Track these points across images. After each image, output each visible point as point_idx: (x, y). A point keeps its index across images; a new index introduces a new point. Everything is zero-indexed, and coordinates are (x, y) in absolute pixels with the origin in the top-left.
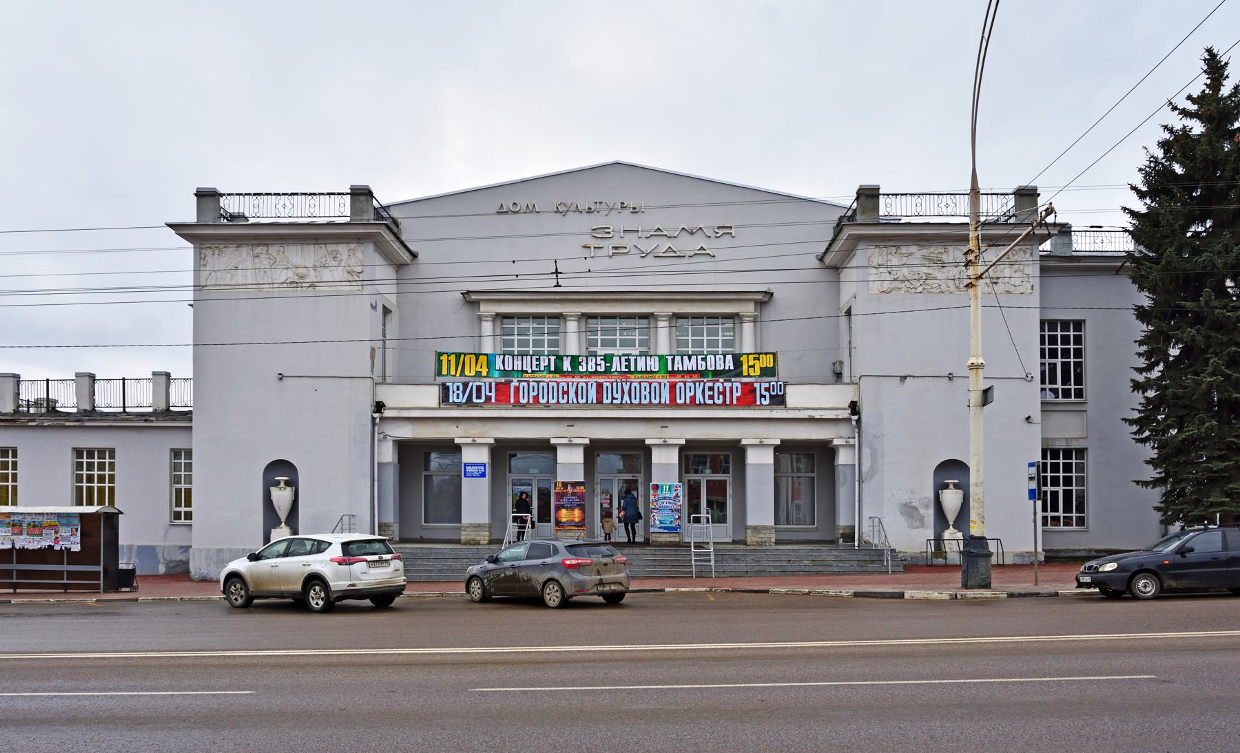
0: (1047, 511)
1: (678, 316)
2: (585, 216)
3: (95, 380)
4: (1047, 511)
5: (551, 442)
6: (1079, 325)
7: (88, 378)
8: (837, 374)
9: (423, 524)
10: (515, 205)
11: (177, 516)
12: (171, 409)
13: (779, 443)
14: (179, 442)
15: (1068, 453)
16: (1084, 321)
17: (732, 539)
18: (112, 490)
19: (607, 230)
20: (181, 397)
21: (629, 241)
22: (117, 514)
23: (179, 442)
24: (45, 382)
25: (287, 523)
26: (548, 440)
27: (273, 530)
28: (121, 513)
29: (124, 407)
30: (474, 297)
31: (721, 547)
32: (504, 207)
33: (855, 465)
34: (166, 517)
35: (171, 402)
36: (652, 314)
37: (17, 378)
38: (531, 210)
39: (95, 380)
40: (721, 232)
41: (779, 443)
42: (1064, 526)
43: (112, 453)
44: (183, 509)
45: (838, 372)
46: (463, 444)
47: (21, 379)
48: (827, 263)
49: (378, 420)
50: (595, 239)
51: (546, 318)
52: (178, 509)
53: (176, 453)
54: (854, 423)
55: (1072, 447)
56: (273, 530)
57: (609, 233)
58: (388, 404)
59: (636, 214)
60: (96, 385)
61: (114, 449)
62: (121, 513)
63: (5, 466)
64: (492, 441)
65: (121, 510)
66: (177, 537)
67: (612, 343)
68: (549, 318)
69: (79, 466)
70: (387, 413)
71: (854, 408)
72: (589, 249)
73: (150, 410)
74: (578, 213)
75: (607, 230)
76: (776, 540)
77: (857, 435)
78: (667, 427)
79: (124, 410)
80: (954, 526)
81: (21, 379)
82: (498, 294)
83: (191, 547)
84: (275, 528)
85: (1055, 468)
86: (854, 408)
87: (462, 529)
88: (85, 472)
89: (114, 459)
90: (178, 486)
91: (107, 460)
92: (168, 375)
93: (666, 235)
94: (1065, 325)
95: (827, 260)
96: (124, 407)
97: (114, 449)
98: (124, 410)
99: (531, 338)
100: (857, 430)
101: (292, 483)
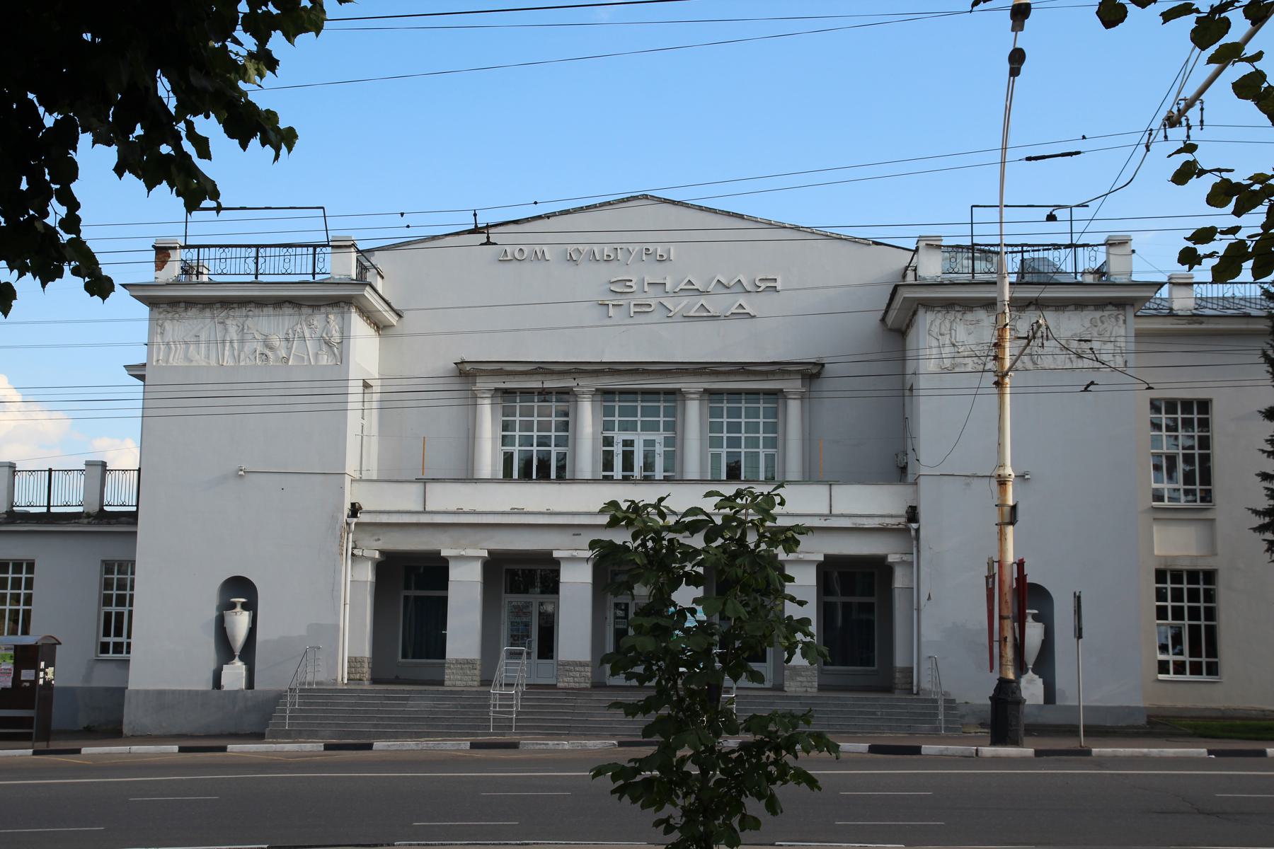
0: (116, 613)
1: (507, 393)
2: (604, 266)
3: (15, 471)
4: (116, 613)
5: (554, 556)
6: (1204, 406)
7: (7, 469)
8: (902, 468)
9: (400, 659)
10: (521, 253)
11: (104, 648)
12: (106, 508)
13: (822, 559)
14: (113, 551)
15: (1193, 576)
16: (1211, 400)
17: (772, 683)
18: (27, 614)
19: (628, 284)
20: (119, 496)
21: (652, 297)
22: (55, 644)
23: (113, 551)
24: (47, 473)
25: (241, 659)
26: (550, 553)
27: (225, 666)
28: (60, 643)
29: (49, 506)
30: (468, 367)
31: (744, 693)
32: (508, 254)
33: (913, 588)
34: (92, 650)
35: (105, 500)
36: (781, 391)
37: (12, 468)
38: (539, 257)
39: (15, 471)
40: (763, 285)
41: (822, 559)
42: (1175, 673)
43: (31, 567)
44: (112, 639)
45: (902, 466)
46: (450, 557)
47: (17, 469)
48: (889, 325)
49: (353, 526)
50: (612, 293)
51: (518, 394)
52: (106, 639)
53: (108, 567)
54: (913, 533)
55: (1199, 568)
56: (225, 666)
57: (631, 287)
58: (365, 508)
59: (663, 263)
60: (16, 477)
61: (34, 560)
62: (60, 643)
63: (1, 584)
64: (486, 554)
65: (60, 641)
66: (103, 678)
67: (630, 427)
68: (746, 394)
69: (108, 585)
70: (362, 518)
71: (913, 514)
72: (605, 307)
73: (80, 509)
74: (571, 263)
75: (628, 284)
76: (818, 685)
77: (915, 550)
78: (580, 534)
79: (49, 509)
80: (1035, 671)
81: (107, 468)
82: (520, 365)
83: (127, 688)
84: (227, 664)
85: (1193, 595)
86: (913, 514)
87: (446, 665)
88: (23, 591)
89: (1158, 607)
90: (108, 609)
91: (24, 576)
92: (104, 464)
93: (698, 289)
94: (1187, 405)
95: (890, 320)
96: (49, 506)
97: (34, 560)
98: (49, 509)
99: (725, 420)
100: (915, 542)
101: (251, 606)
